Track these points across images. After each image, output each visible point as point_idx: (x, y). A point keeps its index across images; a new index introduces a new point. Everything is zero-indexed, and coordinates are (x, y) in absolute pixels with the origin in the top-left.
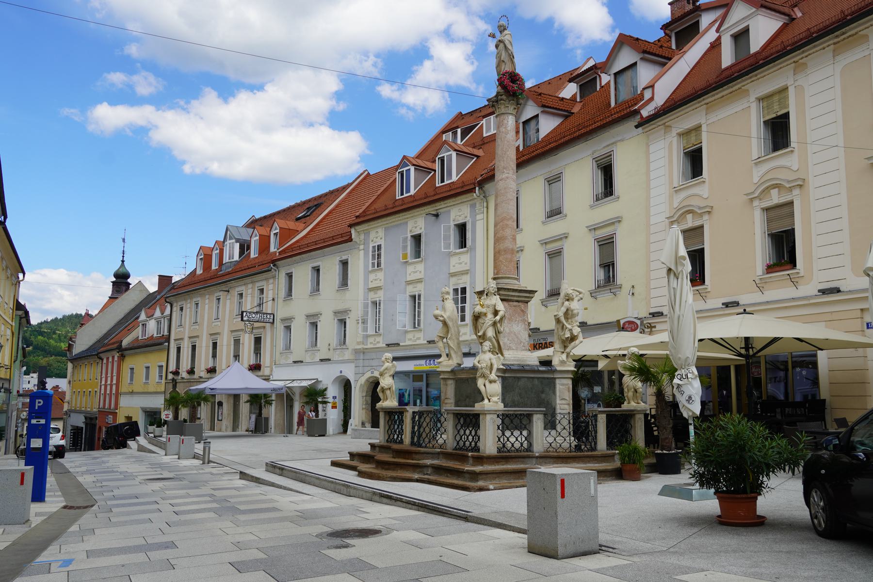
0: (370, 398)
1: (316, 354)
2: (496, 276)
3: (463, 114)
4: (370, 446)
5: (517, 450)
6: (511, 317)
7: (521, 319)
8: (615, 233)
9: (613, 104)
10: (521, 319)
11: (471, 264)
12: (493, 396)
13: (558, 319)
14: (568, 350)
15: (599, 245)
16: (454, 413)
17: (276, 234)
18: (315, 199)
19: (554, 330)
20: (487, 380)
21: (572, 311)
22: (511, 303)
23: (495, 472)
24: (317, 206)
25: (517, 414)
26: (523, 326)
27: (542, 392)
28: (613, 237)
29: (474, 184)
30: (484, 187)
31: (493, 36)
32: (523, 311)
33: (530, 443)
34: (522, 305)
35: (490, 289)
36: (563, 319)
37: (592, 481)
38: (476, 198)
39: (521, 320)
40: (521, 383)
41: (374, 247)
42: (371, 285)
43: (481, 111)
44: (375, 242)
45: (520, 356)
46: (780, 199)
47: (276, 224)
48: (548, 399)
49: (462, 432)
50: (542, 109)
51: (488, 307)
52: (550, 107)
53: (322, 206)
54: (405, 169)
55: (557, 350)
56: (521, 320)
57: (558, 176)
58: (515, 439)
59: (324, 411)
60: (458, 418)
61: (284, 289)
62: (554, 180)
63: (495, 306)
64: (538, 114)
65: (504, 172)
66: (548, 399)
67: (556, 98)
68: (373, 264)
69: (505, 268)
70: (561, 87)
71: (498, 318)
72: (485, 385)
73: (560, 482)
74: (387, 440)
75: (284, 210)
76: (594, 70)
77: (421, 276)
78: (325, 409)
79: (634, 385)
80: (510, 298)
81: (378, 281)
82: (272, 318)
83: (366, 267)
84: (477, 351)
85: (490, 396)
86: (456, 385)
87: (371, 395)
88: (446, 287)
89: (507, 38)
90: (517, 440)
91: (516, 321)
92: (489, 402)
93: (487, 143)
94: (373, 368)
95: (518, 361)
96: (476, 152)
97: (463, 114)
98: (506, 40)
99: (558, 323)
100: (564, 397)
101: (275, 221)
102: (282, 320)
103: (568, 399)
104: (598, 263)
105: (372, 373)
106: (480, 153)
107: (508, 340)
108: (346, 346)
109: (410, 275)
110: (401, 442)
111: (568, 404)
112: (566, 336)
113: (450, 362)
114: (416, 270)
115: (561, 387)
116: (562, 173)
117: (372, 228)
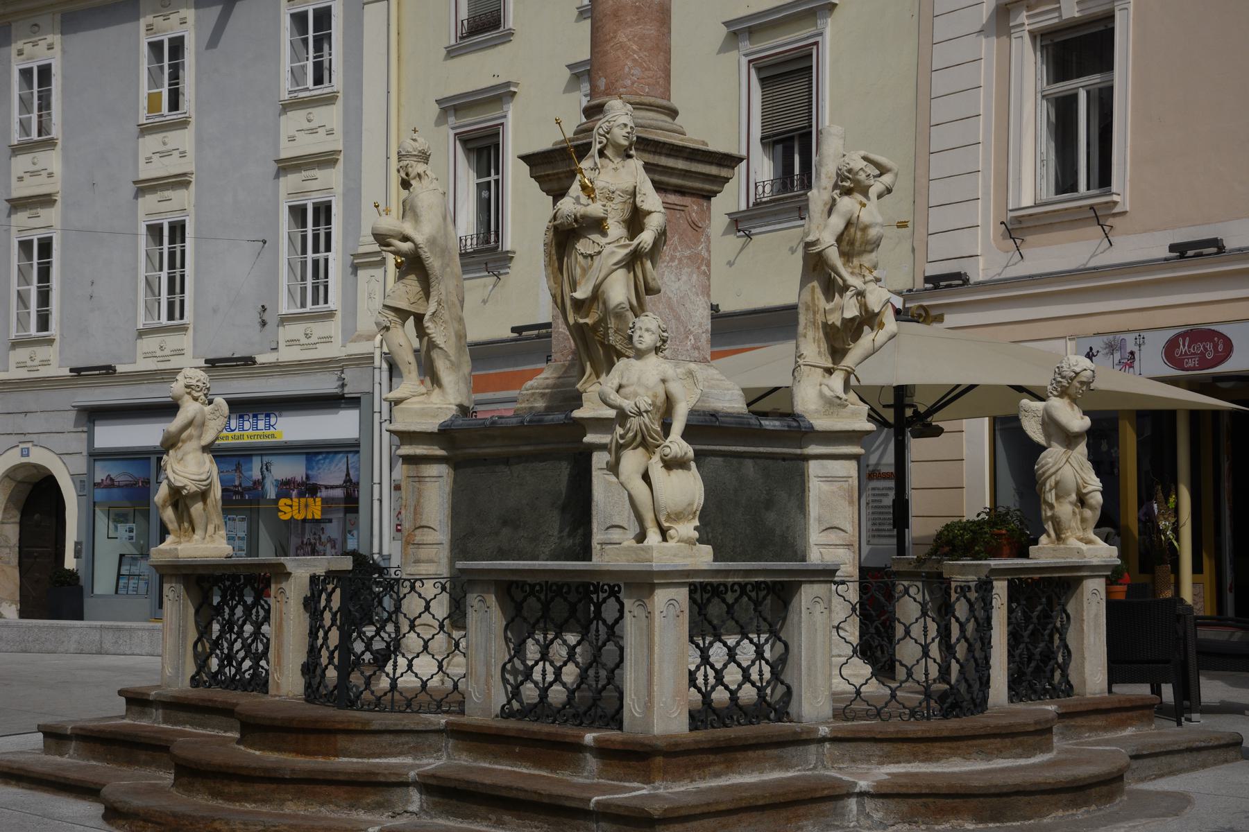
4: (123, 700)
7: (688, 253)
8: (816, 43)
10: (688, 253)
12: (678, 517)
13: (820, 254)
14: (849, 361)
16: (497, 583)
21: (865, 229)
23: (713, 809)
25: (746, 584)
26: (695, 276)
28: (811, 55)
36: (833, 255)
39: (689, 258)
44: (30, 58)
49: (532, 651)
55: (809, 360)
56: (689, 258)
58: (739, 677)
60: (513, 599)
63: (634, 194)
71: (646, 238)
72: (646, 477)
74: (193, 678)
77: (187, 165)
79: (1080, 481)
81: (43, 177)
84: (366, 388)
85: (669, 518)
86: (455, 481)
87: (17, 519)
91: (672, 259)
92: (665, 539)
94: (28, 438)
100: (835, 524)
105: (25, 453)
110: (260, 683)
111: (849, 546)
113: (436, 399)
115: (825, 487)
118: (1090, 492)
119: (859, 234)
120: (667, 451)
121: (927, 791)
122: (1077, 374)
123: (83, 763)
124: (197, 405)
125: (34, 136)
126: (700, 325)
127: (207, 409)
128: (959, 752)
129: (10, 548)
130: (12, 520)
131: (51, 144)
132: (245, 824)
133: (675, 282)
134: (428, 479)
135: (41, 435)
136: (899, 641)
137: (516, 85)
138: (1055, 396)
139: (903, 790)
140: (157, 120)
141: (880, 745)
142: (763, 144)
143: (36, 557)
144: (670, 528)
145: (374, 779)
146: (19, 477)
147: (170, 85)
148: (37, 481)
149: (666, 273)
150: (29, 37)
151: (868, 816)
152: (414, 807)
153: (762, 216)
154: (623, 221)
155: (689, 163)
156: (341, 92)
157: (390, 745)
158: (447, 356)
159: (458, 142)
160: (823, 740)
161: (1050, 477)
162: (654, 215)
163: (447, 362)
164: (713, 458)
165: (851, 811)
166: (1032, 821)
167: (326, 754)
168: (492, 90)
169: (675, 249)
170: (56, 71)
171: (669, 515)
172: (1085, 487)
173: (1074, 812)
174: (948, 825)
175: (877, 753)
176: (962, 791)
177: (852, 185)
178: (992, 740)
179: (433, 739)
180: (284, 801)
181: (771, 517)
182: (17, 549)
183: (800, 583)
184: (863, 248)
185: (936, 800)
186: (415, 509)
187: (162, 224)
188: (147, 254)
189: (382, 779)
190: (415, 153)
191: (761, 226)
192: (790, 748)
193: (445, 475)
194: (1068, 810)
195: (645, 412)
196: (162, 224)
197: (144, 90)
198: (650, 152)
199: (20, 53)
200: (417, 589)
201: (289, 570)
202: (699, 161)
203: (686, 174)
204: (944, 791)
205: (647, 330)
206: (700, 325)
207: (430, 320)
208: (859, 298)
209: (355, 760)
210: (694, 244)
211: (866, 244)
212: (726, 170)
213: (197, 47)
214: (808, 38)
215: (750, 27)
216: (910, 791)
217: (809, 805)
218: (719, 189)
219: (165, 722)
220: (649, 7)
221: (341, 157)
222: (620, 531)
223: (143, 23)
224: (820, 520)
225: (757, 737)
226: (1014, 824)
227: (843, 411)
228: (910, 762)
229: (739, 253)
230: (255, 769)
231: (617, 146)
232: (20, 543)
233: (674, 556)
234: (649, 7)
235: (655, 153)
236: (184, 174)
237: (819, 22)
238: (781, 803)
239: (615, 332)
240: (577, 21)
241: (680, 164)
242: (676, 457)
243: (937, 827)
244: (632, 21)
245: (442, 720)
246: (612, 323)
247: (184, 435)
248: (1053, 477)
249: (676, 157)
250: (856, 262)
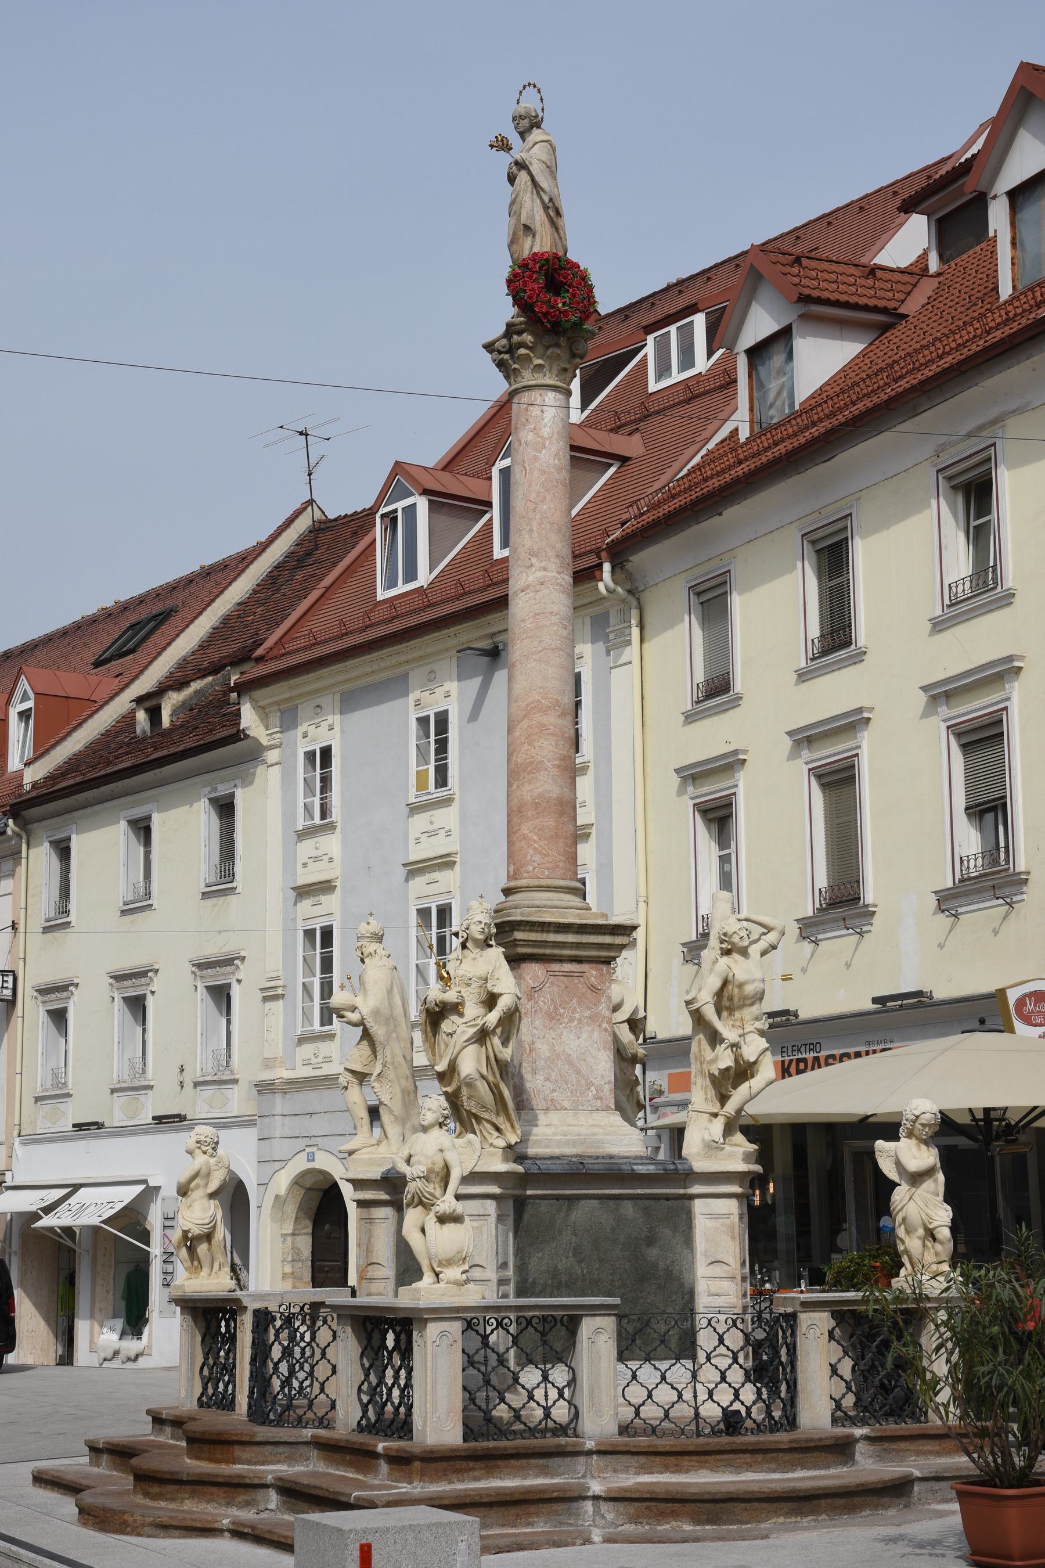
0: (309, 1240)
1: (143, 1098)
2: (513, 884)
3: (602, 314)
4: (150, 1418)
5: (532, 1432)
6: (556, 1008)
7: (588, 1013)
9: (1006, 290)
10: (588, 1013)
12: (449, 1262)
13: (698, 1010)
17: (24, 715)
18: (156, 594)
20: (432, 1214)
22: (555, 967)
24: (162, 618)
27: (651, 1241)
29: (598, 552)
30: (628, 561)
31: (502, 145)
32: (594, 989)
33: (576, 1407)
34: (591, 972)
35: (473, 927)
36: (710, 1012)
37: (463, 1546)
38: (605, 598)
39: (590, 1017)
40: (582, 1212)
41: (310, 756)
42: (305, 878)
43: (653, 304)
45: (583, 1130)
47: (24, 684)
48: (668, 1262)
50: (802, 309)
51: (468, 985)
52: (828, 302)
53: (175, 621)
54: (400, 505)
57: (839, 525)
59: (168, 1285)
60: (365, 1330)
61: (45, 891)
64: (791, 324)
65: (532, 565)
66: (668, 1262)
67: (852, 270)
68: (421, 776)
69: (537, 858)
70: (885, 230)
72: (423, 1230)
73: (357, 1554)
75: (48, 640)
78: (169, 1278)
80: (548, 951)
82: (10, 985)
83: (288, 816)
85: (440, 1264)
87: (310, 1230)
88: (371, 919)
89: (535, 155)
90: (531, 1397)
91: (571, 1020)
93: (658, 413)
94: (313, 1141)
95: (574, 1144)
96: (621, 444)
97: (602, 314)
98: (534, 161)
99: (699, 1024)
101: (20, 672)
102: (39, 991)
103: (731, 1261)
104: (960, 802)
105: (311, 1158)
106: (631, 445)
107: (547, 1079)
108: (232, 1072)
109: (305, 865)
111: (733, 1278)
112: (723, 1065)
114: (436, 826)
115: (710, 1223)
116: (850, 515)
117: (301, 696)
118: (936, 1228)
119: (736, 991)
120: (438, 1209)
121: (648, 1496)
122: (917, 1117)
123: (111, 1473)
124: (206, 1157)
125: (317, 820)
126: (602, 1077)
127: (212, 1161)
128: (707, 1465)
129: (302, 1261)
130: (305, 1231)
131: (331, 827)
132: (143, 1516)
133: (574, 1040)
134: (377, 1221)
135: (325, 1138)
136: (654, 1366)
137: (745, 752)
138: (904, 1137)
139: (628, 1495)
140: (425, 798)
141: (636, 1458)
142: (969, 815)
143: (327, 1272)
144: (441, 1272)
145: (242, 1481)
146: (308, 1185)
147: (436, 761)
148: (327, 1187)
149: (565, 1033)
150: (312, 718)
151: (603, 1517)
152: (272, 1506)
153: (966, 894)
154: (482, 1002)
155: (579, 936)
156: (592, 761)
157: (271, 1454)
158: (391, 1112)
159: (696, 813)
160: (590, 1453)
161: (898, 1213)
162: (503, 997)
163: (392, 1117)
164: (588, 1201)
165: (586, 1512)
166: (750, 1526)
167: (227, 1462)
168: (722, 759)
169: (574, 1011)
170: (335, 752)
171: (440, 1261)
172: (930, 1223)
173: (799, 1519)
174: (668, 1526)
175: (634, 1464)
176: (678, 1497)
177: (729, 947)
178: (741, 1455)
179: (303, 1449)
180: (183, 1499)
181: (653, 1253)
182: (310, 1263)
183: (582, 1316)
184: (742, 1002)
185: (659, 1504)
186: (367, 1248)
187: (430, 908)
188: (418, 940)
189: (248, 1481)
190: (369, 935)
191: (966, 905)
192: (556, 1459)
193: (390, 1216)
194: (789, 1518)
195: (418, 1177)
196: (430, 908)
197: (413, 768)
198: (537, 931)
199: (305, 736)
200: (329, 1323)
201: (245, 1304)
202: (590, 933)
203: (578, 945)
204: (662, 1496)
205: (429, 1109)
206: (602, 1077)
207: (375, 1081)
208: (734, 1049)
209: (246, 1467)
210: (595, 1005)
211: (744, 999)
212: (620, 937)
213: (460, 719)
214: (998, 703)
215: (946, 691)
216: (633, 1496)
217: (541, 1505)
218: (617, 954)
219: (173, 1438)
220: (547, 802)
221: (593, 831)
222: (481, 1269)
223: (412, 697)
224: (706, 1254)
225: (516, 1448)
226: (731, 1527)
227: (720, 1154)
228: (662, 1473)
229: (950, 931)
230: (165, 1473)
231: (476, 941)
232: (312, 1256)
233: (442, 1295)
234: (547, 802)
235: (542, 931)
236: (449, 855)
237: (1007, 686)
238: (507, 1501)
239: (469, 1098)
240: (797, 684)
241: (570, 938)
242: (445, 1213)
243: (659, 1528)
244: (533, 815)
245: (308, 1433)
246: (465, 1091)
247: (193, 1185)
248: (900, 1214)
249: (566, 932)
250: (737, 1014)
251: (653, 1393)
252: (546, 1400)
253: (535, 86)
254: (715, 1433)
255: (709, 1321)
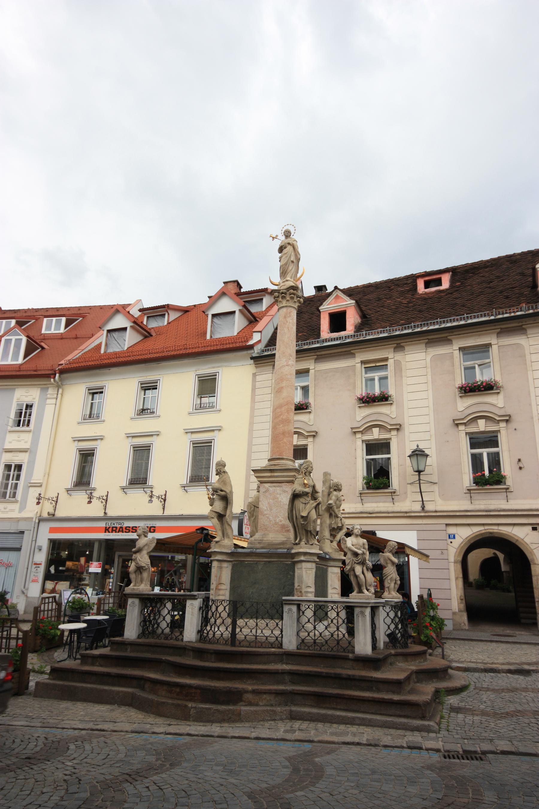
8: (214, 439)
11: (32, 443)
15: (194, 447)
19: (33, 518)
46: (298, 442)
50: (132, 324)
62: (96, 392)
76: (166, 308)
111: (338, 594)
251: (225, 630)
252: (315, 636)
253: (295, 227)
254: (226, 644)
255: (332, 607)
